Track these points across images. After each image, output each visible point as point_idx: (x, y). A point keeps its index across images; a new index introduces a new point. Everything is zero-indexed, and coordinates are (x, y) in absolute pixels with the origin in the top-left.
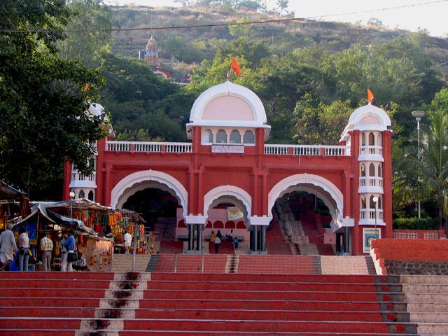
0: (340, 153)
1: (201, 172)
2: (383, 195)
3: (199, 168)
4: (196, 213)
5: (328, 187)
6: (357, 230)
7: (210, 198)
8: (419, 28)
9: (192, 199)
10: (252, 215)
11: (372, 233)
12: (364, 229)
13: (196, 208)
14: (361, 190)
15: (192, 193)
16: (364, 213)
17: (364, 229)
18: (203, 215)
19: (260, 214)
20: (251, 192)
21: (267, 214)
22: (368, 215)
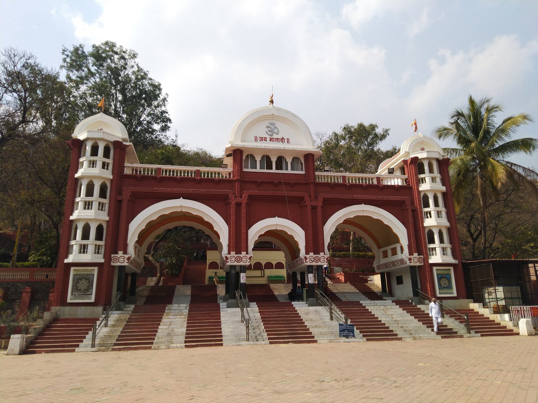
3: (241, 197)
6: (427, 269)
12: (435, 268)
17: (435, 268)
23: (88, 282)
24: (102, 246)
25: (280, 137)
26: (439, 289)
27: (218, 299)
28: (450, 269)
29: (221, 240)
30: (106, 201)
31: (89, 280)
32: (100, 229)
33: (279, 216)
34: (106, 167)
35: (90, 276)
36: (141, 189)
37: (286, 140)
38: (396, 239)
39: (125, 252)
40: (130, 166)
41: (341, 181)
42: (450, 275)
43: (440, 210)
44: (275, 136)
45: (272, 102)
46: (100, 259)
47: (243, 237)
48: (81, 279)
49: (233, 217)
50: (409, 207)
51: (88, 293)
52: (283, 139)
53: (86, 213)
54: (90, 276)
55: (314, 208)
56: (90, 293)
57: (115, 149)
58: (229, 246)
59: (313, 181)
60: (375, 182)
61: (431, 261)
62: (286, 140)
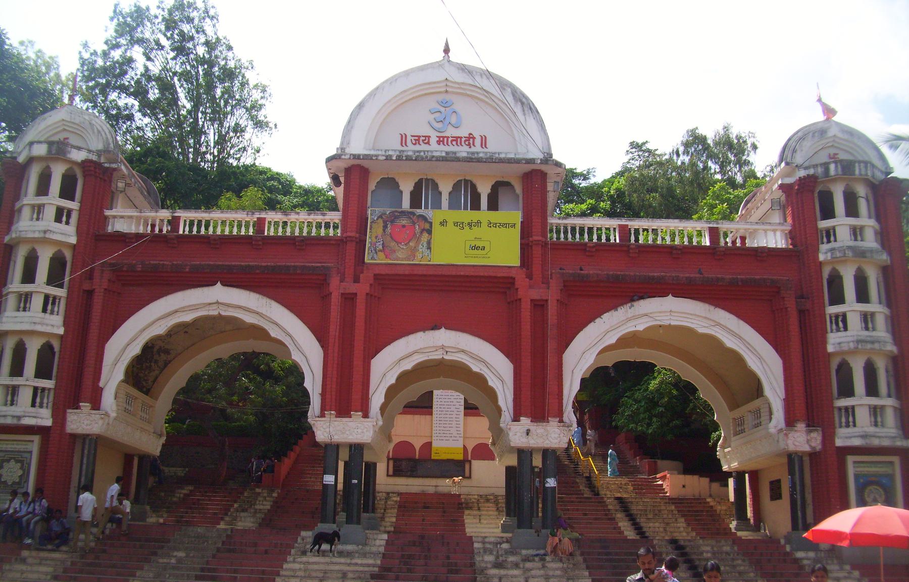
0: (574, 235)
1: (361, 289)
3: (356, 280)
4: (343, 411)
7: (389, 364)
8: (86, 45)
10: (516, 419)
11: (873, 469)
12: (850, 459)
13: (346, 395)
14: (835, 341)
15: (527, 362)
16: (850, 411)
17: (850, 459)
18: (366, 416)
19: (540, 415)
20: (510, 350)
21: (560, 414)
22: (863, 416)
24: (49, 389)
25: (463, 133)
27: (518, 226)
28: (891, 463)
29: (307, 384)
32: (46, 352)
33: (424, 329)
34: (64, 219)
36: (591, 270)
37: (478, 142)
38: (756, 389)
40: (127, 217)
41: (616, 238)
42: (891, 477)
43: (872, 310)
44: (451, 132)
45: (447, 51)
46: (44, 418)
48: (8, 461)
49: (334, 330)
50: (791, 304)
52: (470, 138)
55: (349, 299)
57: (85, 176)
58: (323, 395)
59: (540, 238)
60: (706, 242)
61: (839, 443)
62: (478, 142)
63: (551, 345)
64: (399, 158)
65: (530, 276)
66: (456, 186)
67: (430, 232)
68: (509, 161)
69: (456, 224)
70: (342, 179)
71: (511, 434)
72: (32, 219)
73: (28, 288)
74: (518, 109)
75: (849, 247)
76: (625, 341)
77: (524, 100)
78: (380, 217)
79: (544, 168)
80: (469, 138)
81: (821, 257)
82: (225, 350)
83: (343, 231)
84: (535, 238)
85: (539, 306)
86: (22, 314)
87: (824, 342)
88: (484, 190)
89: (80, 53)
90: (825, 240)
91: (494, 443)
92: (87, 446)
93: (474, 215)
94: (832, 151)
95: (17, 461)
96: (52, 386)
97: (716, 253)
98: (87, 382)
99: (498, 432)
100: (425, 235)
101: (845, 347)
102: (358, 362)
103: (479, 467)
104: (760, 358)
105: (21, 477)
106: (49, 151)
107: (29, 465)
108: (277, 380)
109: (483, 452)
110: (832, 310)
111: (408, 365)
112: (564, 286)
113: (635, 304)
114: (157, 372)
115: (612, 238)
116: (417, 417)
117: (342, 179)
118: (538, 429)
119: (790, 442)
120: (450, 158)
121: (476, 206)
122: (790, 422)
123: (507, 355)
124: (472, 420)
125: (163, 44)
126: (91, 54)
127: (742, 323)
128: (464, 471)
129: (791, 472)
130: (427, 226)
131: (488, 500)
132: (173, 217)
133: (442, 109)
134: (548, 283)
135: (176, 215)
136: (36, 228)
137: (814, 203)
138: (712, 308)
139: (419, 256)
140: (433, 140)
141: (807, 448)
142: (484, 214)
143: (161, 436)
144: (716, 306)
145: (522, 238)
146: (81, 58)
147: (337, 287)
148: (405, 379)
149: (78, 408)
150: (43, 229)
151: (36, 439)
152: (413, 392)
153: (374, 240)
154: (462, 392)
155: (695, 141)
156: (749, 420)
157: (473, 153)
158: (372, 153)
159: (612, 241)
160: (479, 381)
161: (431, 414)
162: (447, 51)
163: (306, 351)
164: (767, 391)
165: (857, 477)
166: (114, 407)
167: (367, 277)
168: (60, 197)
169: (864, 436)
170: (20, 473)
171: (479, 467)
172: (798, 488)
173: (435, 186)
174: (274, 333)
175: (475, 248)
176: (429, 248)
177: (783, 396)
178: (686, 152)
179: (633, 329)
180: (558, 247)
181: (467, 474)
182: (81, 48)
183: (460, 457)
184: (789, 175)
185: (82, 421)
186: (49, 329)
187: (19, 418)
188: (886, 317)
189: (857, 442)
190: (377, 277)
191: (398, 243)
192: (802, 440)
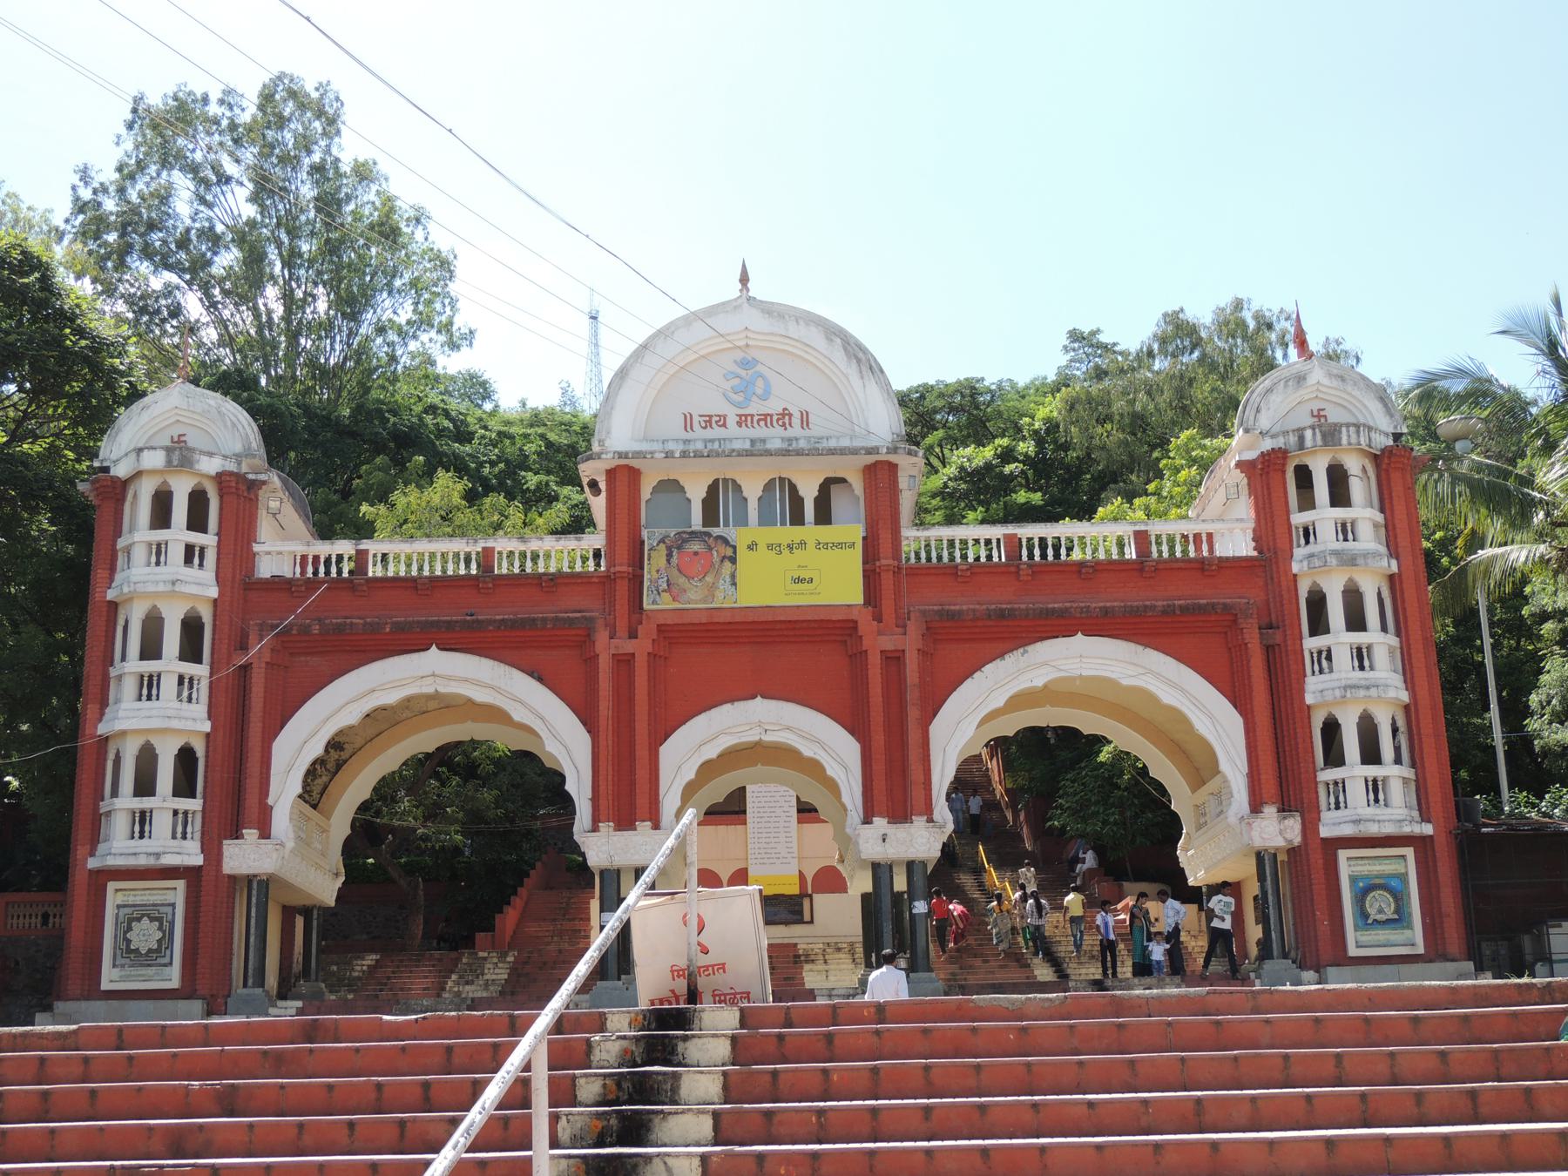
1: (640, 647)
2: (1407, 708)
3: (633, 635)
4: (625, 822)
5: (1175, 686)
6: (1317, 859)
7: (684, 753)
8: (85, 175)
9: (879, 767)
10: (867, 821)
11: (1377, 868)
12: (1343, 855)
13: (630, 800)
14: (1317, 690)
15: (879, 739)
16: (1340, 785)
17: (1343, 855)
19: (900, 815)
20: (856, 726)
21: (928, 811)
22: (1356, 793)
23: (160, 928)
26: (1356, 929)
28: (1403, 857)
29: (570, 787)
30: (201, 671)
31: (130, 921)
32: (186, 757)
34: (196, 560)
35: (163, 909)
36: (963, 603)
37: (796, 421)
39: (265, 834)
42: (1403, 877)
44: (755, 408)
45: (744, 279)
46: (191, 854)
47: (642, 774)
48: (139, 920)
49: (605, 708)
51: (161, 961)
53: (153, 711)
54: (163, 909)
55: (624, 662)
56: (166, 960)
58: (595, 800)
59: (891, 562)
60: (1131, 553)
61: (1325, 832)
62: (796, 421)
63: (913, 713)
64: (684, 454)
65: (878, 618)
66: (769, 486)
67: (733, 560)
68: (842, 452)
69: (770, 547)
70: (603, 486)
71: (861, 842)
72: (149, 564)
73: (151, 666)
74: (852, 370)
75: (1335, 553)
76: (1018, 701)
77: (861, 355)
78: (662, 541)
79: (892, 458)
80: (783, 415)
81: (1295, 568)
82: (426, 741)
83: (610, 565)
84: (884, 562)
85: (894, 660)
86: (145, 704)
87: (1302, 691)
88: (809, 492)
89: (74, 188)
90: (1302, 541)
91: (842, 860)
92: (254, 892)
93: (796, 533)
94: (1315, 406)
95: (152, 919)
96: (200, 808)
97: (1144, 568)
98: (251, 800)
99: (846, 843)
100: (727, 564)
101: (1329, 696)
102: (642, 752)
103: (823, 904)
104: (1211, 717)
105: (159, 941)
106: (169, 462)
107: (172, 923)
108: (485, 781)
109: (831, 880)
110: (1311, 643)
111: (711, 752)
112: (928, 629)
113: (1030, 648)
114: (325, 779)
115: (995, 554)
116: (722, 828)
117: (603, 486)
118: (898, 832)
119: (1255, 834)
120: (756, 451)
121: (797, 519)
122: (1256, 808)
123: (852, 732)
124: (810, 828)
125: (229, 173)
126: (95, 192)
127: (1183, 667)
128: (801, 913)
129: (1261, 877)
130: (729, 552)
131: (839, 950)
132: (359, 552)
133: (743, 373)
134: (905, 626)
135: (362, 547)
136: (158, 578)
137: (1285, 483)
138: (1140, 648)
139: (719, 595)
140: (732, 421)
141: (1279, 842)
142: (810, 531)
143: (337, 875)
144: (1146, 645)
145: (865, 562)
146: (77, 199)
147: (605, 647)
148: (708, 770)
149: (238, 836)
150: (171, 578)
151: (180, 884)
152: (717, 790)
153: (655, 575)
154: (792, 786)
155: (1178, 332)
156: (1211, 808)
157: (790, 440)
158: (645, 447)
159: (996, 559)
160: (813, 768)
161: (744, 823)
162: (744, 279)
163: (566, 744)
164: (1224, 765)
165: (1354, 880)
166: (291, 835)
167: (647, 631)
168: (189, 528)
169: (1357, 822)
170: (159, 935)
171: (823, 904)
172: (1270, 898)
173: (738, 488)
174: (518, 715)
175: (799, 580)
176: (734, 584)
177: (1245, 769)
178: (1164, 352)
179: (1029, 684)
180: (915, 572)
181: (807, 917)
182: (75, 179)
183: (795, 890)
184: (1251, 448)
185: (244, 856)
186: (190, 726)
187: (158, 855)
188: (1391, 651)
189: (1347, 831)
190: (661, 628)
191: (689, 578)
192: (1276, 831)
